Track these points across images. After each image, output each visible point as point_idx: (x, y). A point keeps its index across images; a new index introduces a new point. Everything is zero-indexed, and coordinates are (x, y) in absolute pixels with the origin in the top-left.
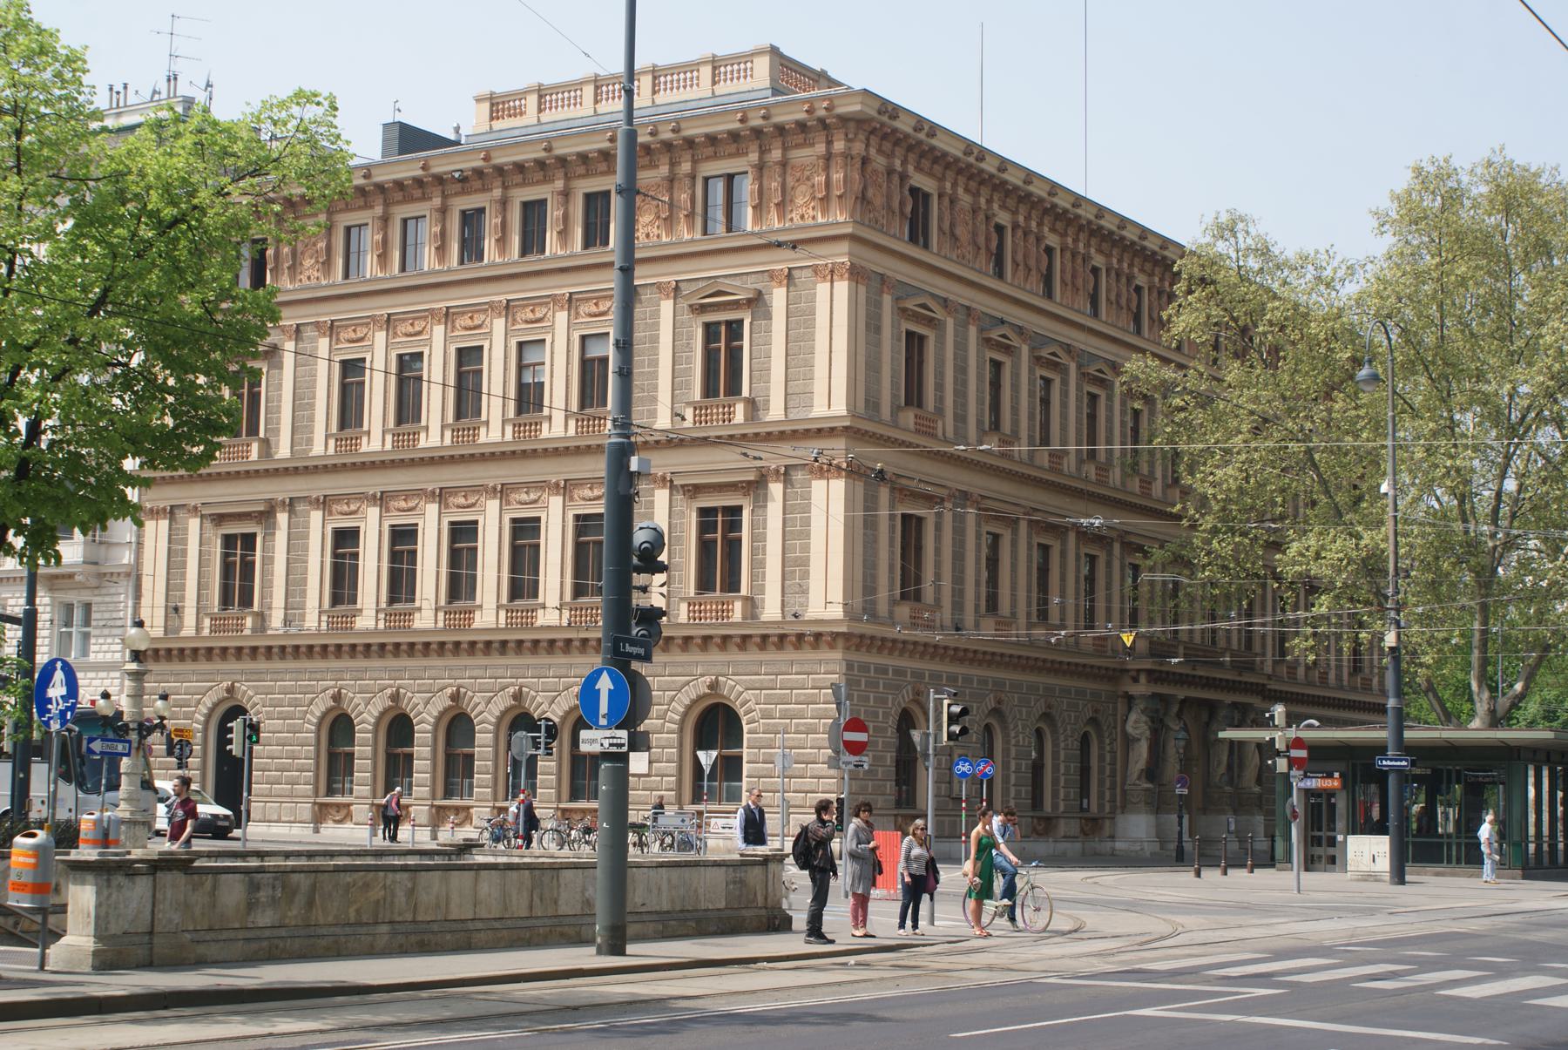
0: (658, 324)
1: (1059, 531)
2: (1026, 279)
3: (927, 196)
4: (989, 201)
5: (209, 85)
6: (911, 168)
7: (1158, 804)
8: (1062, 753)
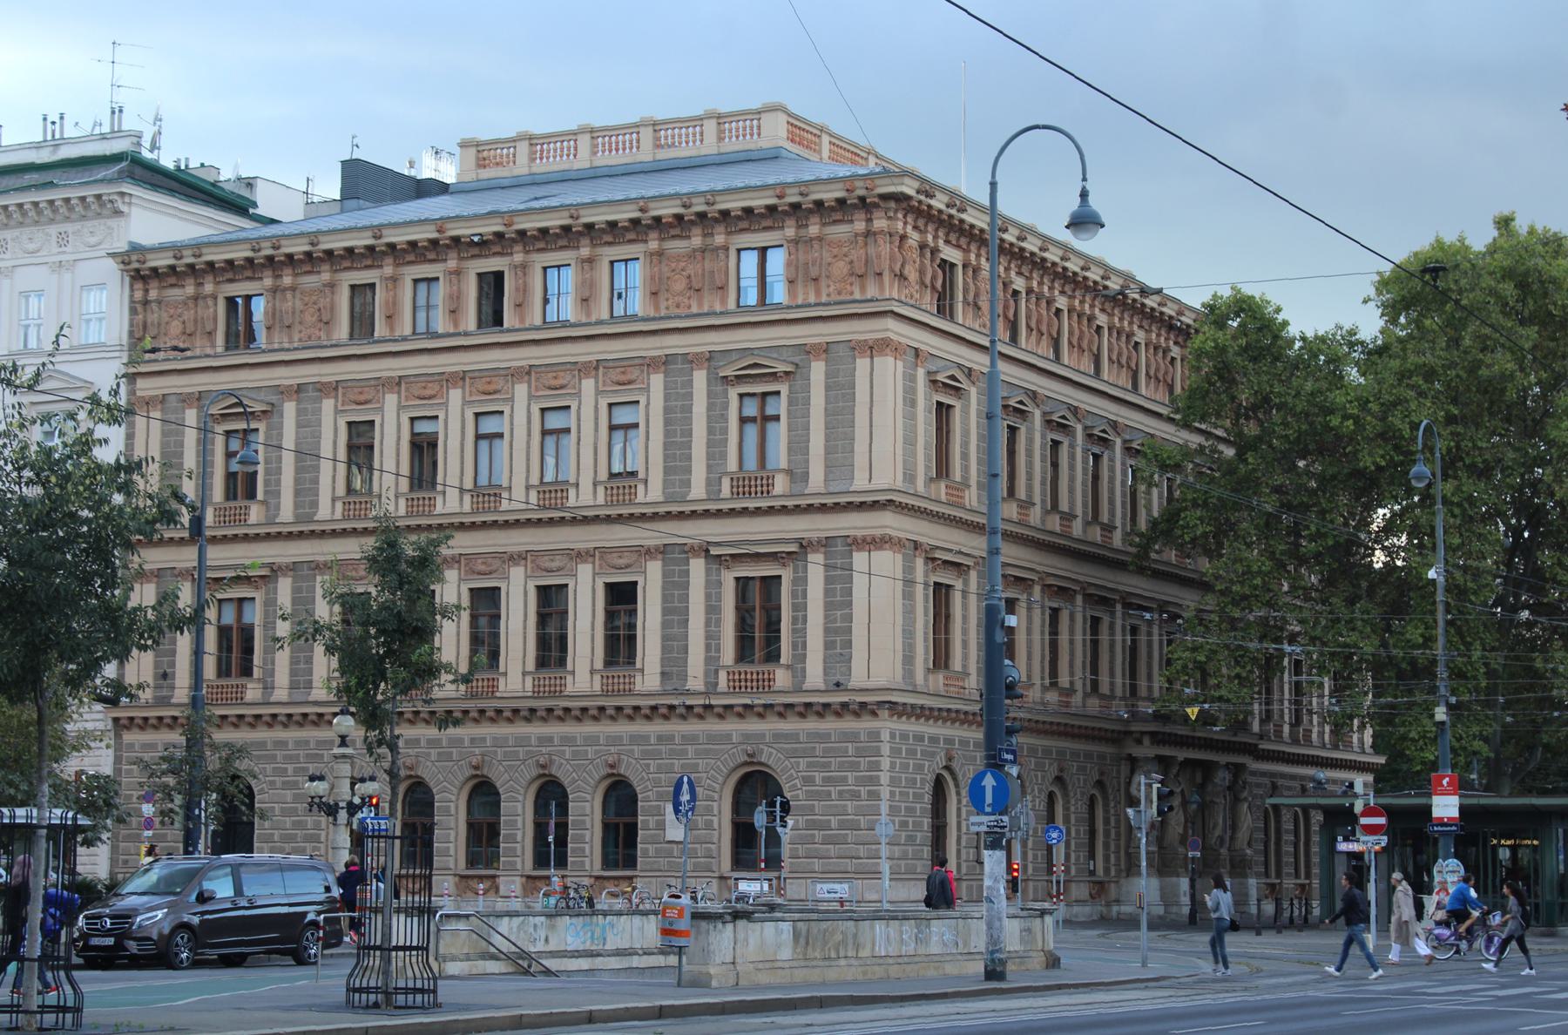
0: (691, 394)
1: (1105, 602)
2: (1038, 342)
3: (953, 265)
4: (1007, 269)
5: (158, 119)
6: (941, 242)
7: (1164, 865)
8: (1073, 817)
